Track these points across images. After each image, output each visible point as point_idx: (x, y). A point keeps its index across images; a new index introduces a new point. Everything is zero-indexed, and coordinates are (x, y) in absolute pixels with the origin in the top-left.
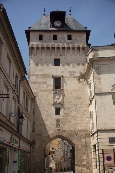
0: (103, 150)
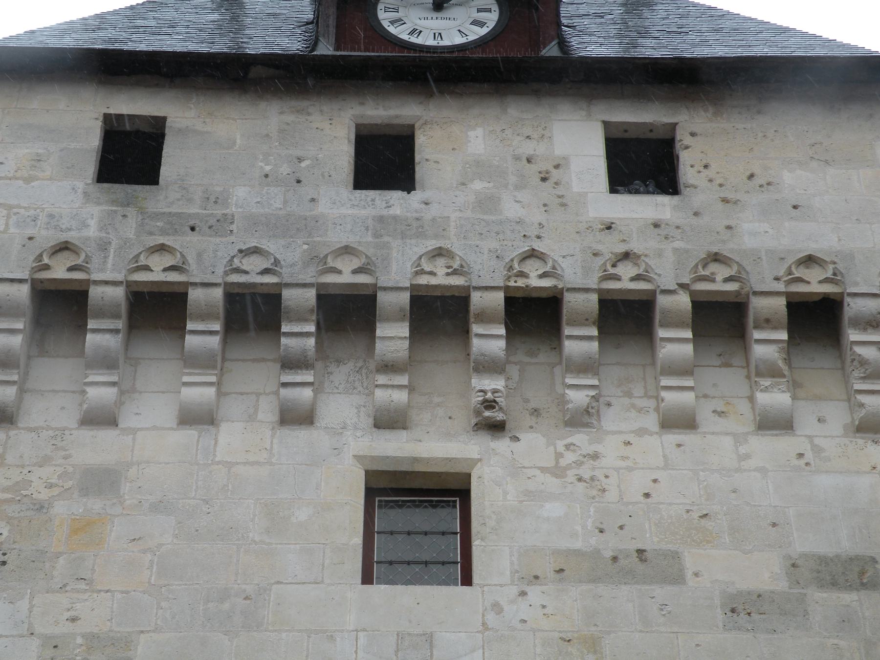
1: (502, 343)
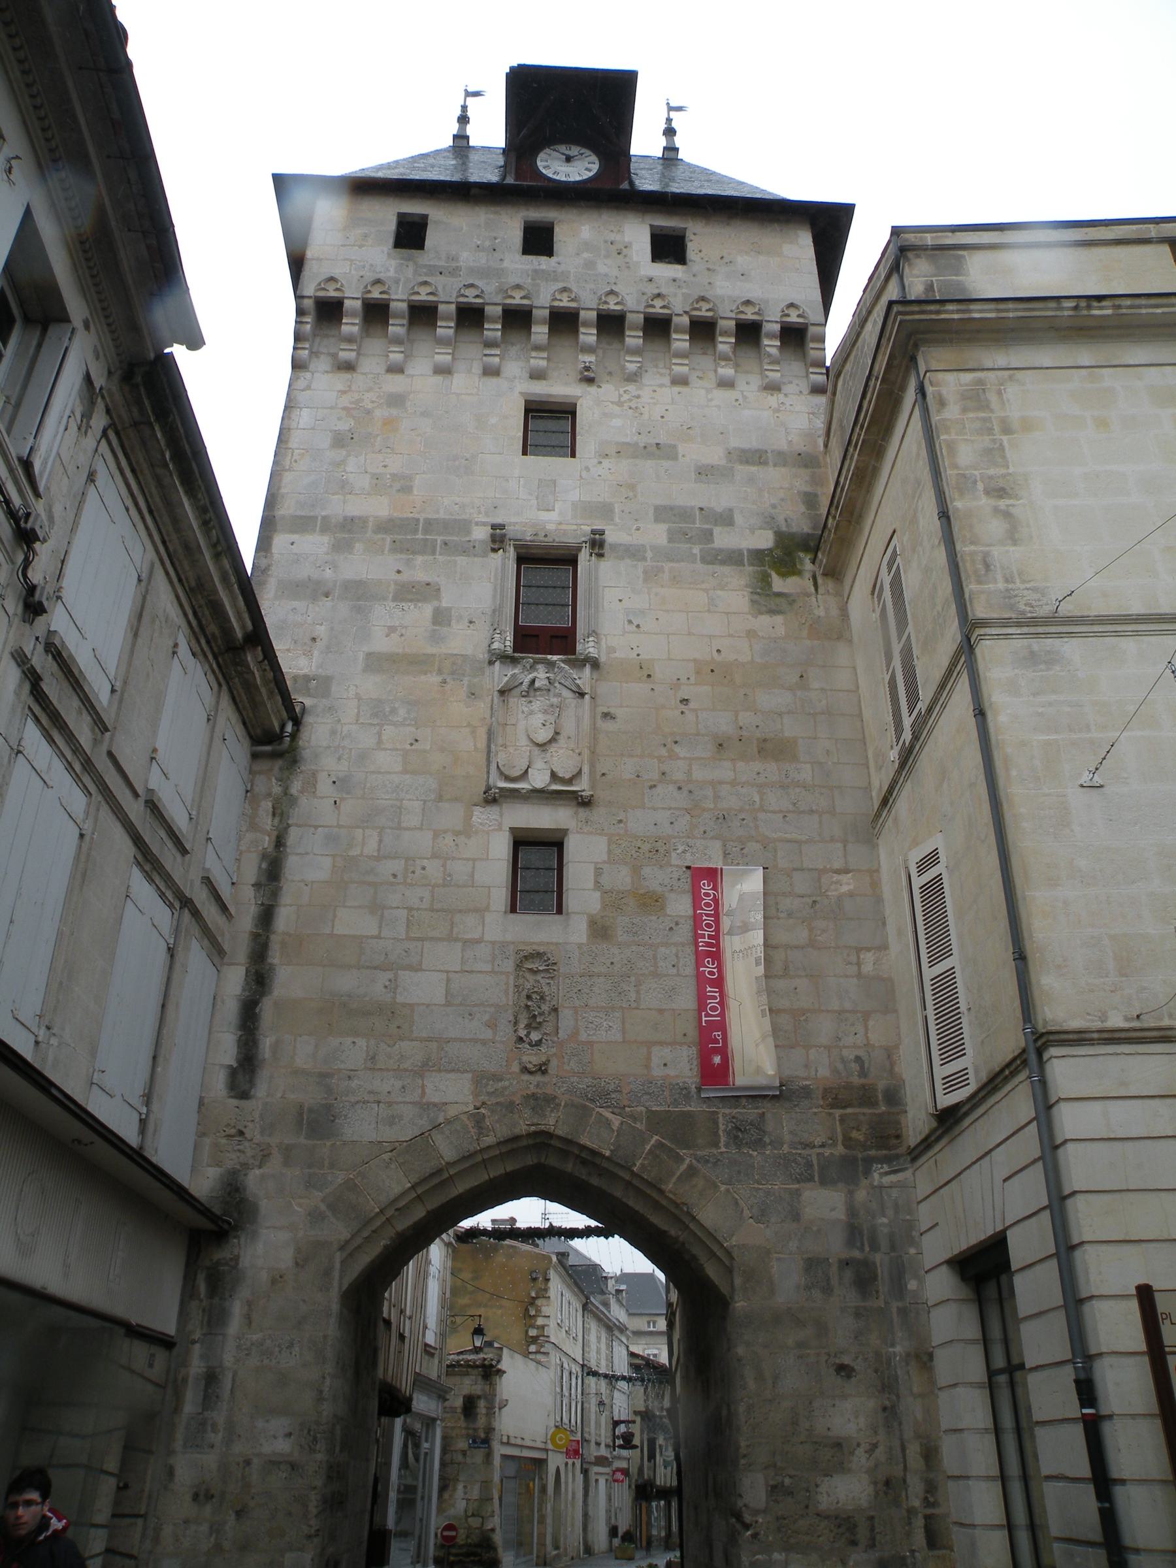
0: (1145, 1294)
1: (595, 338)
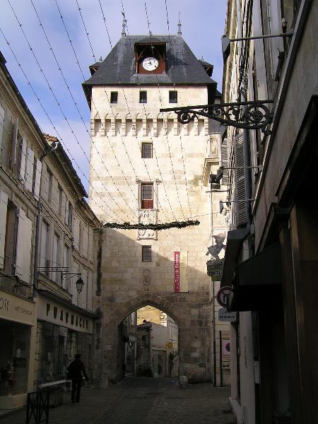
0: (220, 332)
